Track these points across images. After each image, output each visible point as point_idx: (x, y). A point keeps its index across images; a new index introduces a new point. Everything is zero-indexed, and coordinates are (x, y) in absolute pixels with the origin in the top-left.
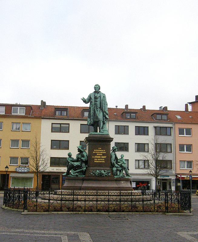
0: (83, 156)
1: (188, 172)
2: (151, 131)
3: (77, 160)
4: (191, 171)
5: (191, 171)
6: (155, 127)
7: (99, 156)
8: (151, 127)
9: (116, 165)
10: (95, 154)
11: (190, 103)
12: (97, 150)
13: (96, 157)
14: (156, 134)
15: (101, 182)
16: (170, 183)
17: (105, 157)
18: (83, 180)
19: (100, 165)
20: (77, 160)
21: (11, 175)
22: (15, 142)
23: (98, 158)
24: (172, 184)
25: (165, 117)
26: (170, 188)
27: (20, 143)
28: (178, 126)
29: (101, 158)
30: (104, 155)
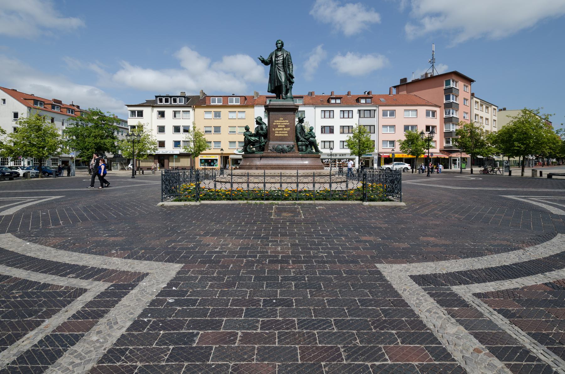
0: (262, 129)
1: (390, 151)
2: (356, 115)
3: (255, 135)
4: (393, 150)
5: (393, 150)
6: (359, 111)
7: (282, 126)
8: (355, 110)
9: (302, 139)
10: (276, 126)
11: (394, 87)
12: (277, 121)
13: (277, 129)
14: (383, 144)
15: (267, 159)
16: (373, 161)
17: (288, 129)
18: (261, 157)
19: (282, 139)
20: (255, 135)
21: (231, 156)
22: (177, 129)
23: (279, 131)
24: (374, 162)
25: (369, 100)
26: (373, 165)
27: (182, 129)
28: (381, 108)
29: (283, 131)
30: (286, 126)
